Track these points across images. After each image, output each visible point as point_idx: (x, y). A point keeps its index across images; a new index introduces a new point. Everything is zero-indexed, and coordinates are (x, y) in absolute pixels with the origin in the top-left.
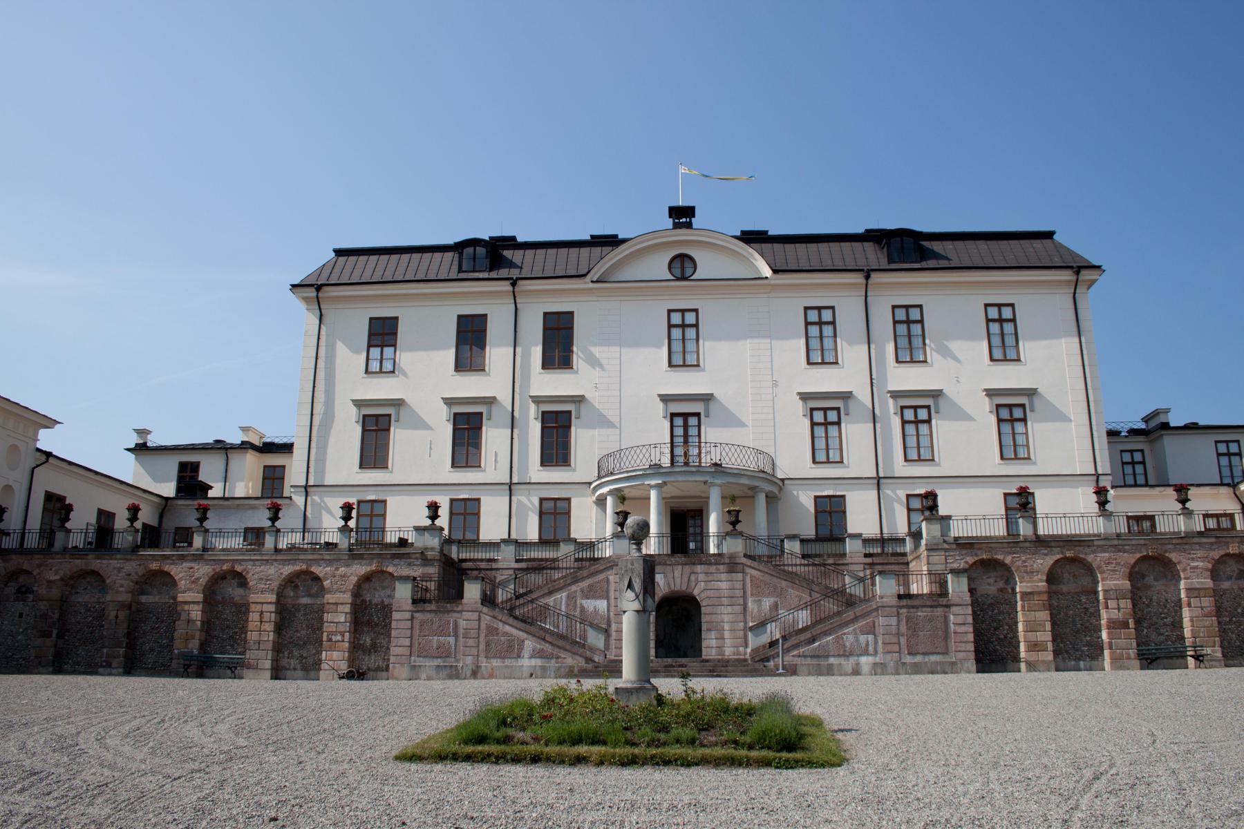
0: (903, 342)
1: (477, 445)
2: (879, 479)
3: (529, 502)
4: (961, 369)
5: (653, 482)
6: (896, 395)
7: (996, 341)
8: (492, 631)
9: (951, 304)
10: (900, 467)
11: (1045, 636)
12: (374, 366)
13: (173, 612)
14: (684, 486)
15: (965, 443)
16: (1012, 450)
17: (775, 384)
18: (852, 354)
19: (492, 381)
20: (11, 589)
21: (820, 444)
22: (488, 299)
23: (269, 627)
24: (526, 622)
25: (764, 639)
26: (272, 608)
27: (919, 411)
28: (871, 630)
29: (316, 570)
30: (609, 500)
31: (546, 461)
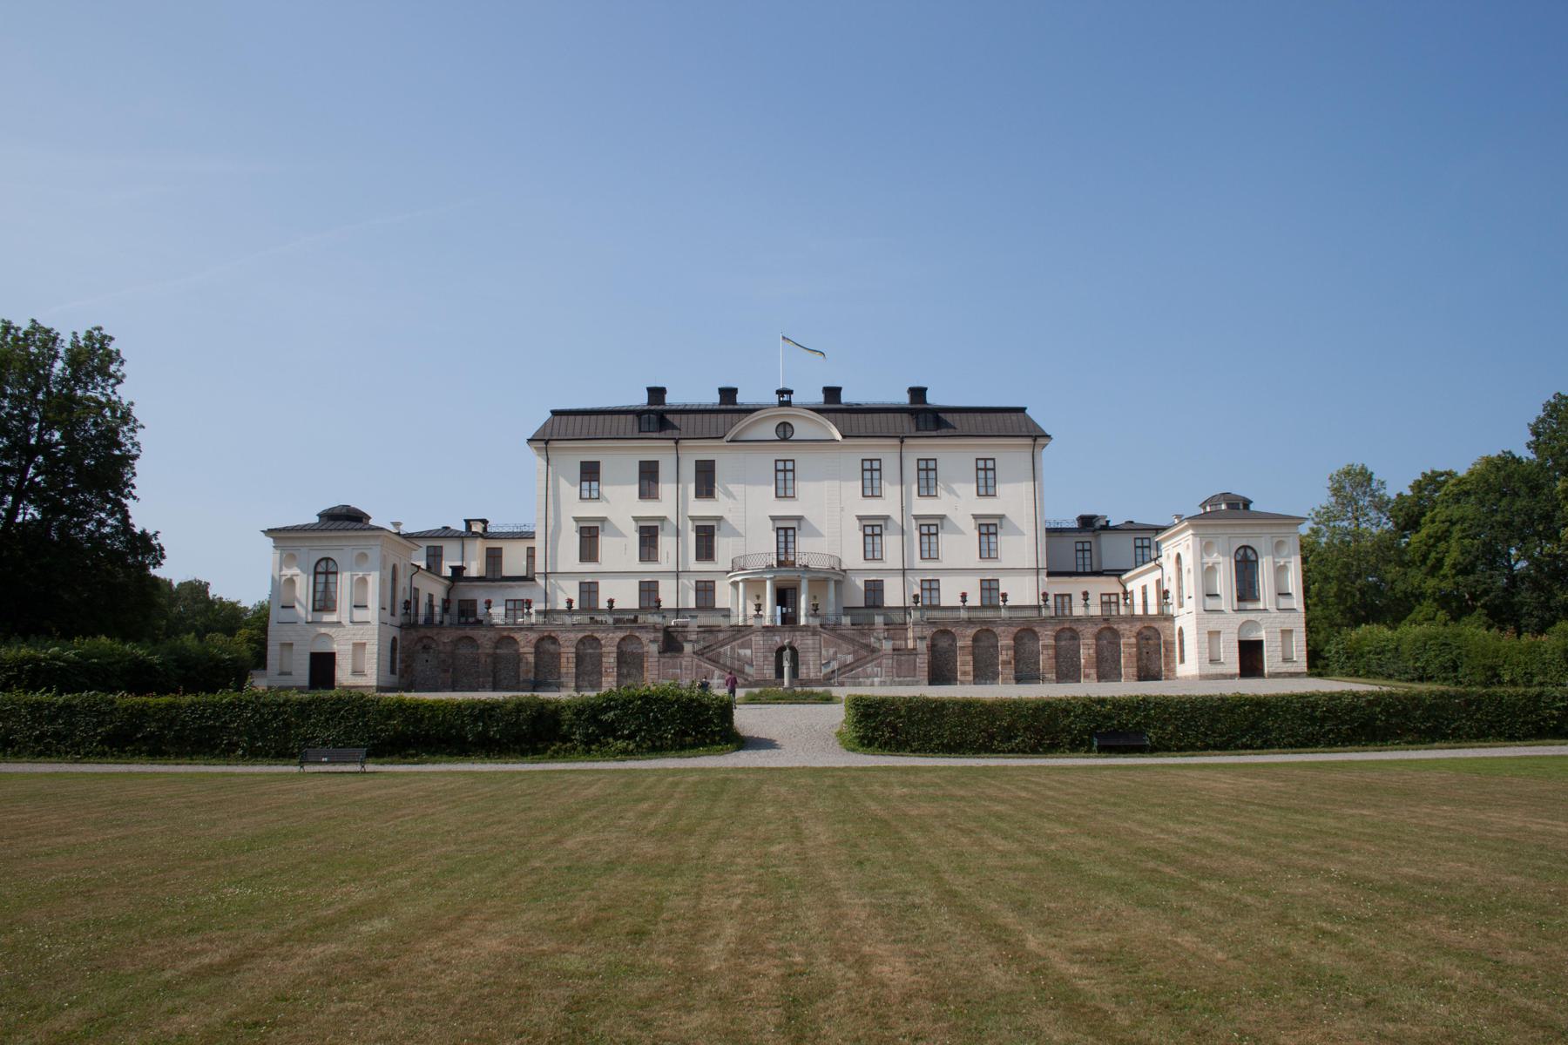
0: (923, 483)
1: (656, 547)
3: (689, 583)
4: (959, 502)
6: (917, 517)
7: (982, 482)
8: (699, 666)
9: (954, 458)
10: (918, 563)
11: (970, 668)
12: (586, 494)
13: (518, 658)
14: (786, 575)
15: (959, 548)
16: (987, 552)
17: (842, 509)
18: (891, 491)
19: (663, 506)
20: (419, 647)
21: (869, 548)
22: (660, 452)
24: (714, 661)
25: (829, 670)
27: (931, 528)
28: (880, 665)
31: (699, 558)
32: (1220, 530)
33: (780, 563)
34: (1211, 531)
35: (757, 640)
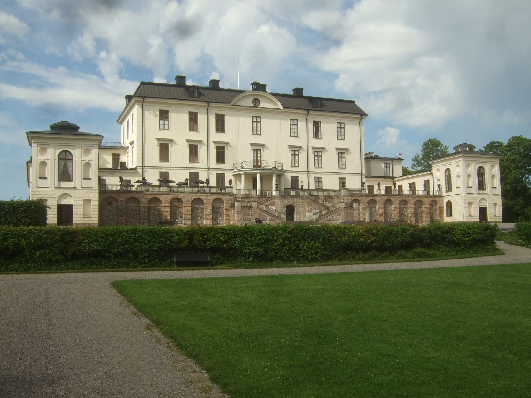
2: (308, 172)
5: (259, 172)
19: (199, 136)
23: (190, 213)
26: (190, 208)
27: (318, 151)
28: (339, 215)
29: (201, 197)
30: (243, 176)
32: (488, 160)
33: (254, 166)
34: (470, 159)
35: (277, 202)
